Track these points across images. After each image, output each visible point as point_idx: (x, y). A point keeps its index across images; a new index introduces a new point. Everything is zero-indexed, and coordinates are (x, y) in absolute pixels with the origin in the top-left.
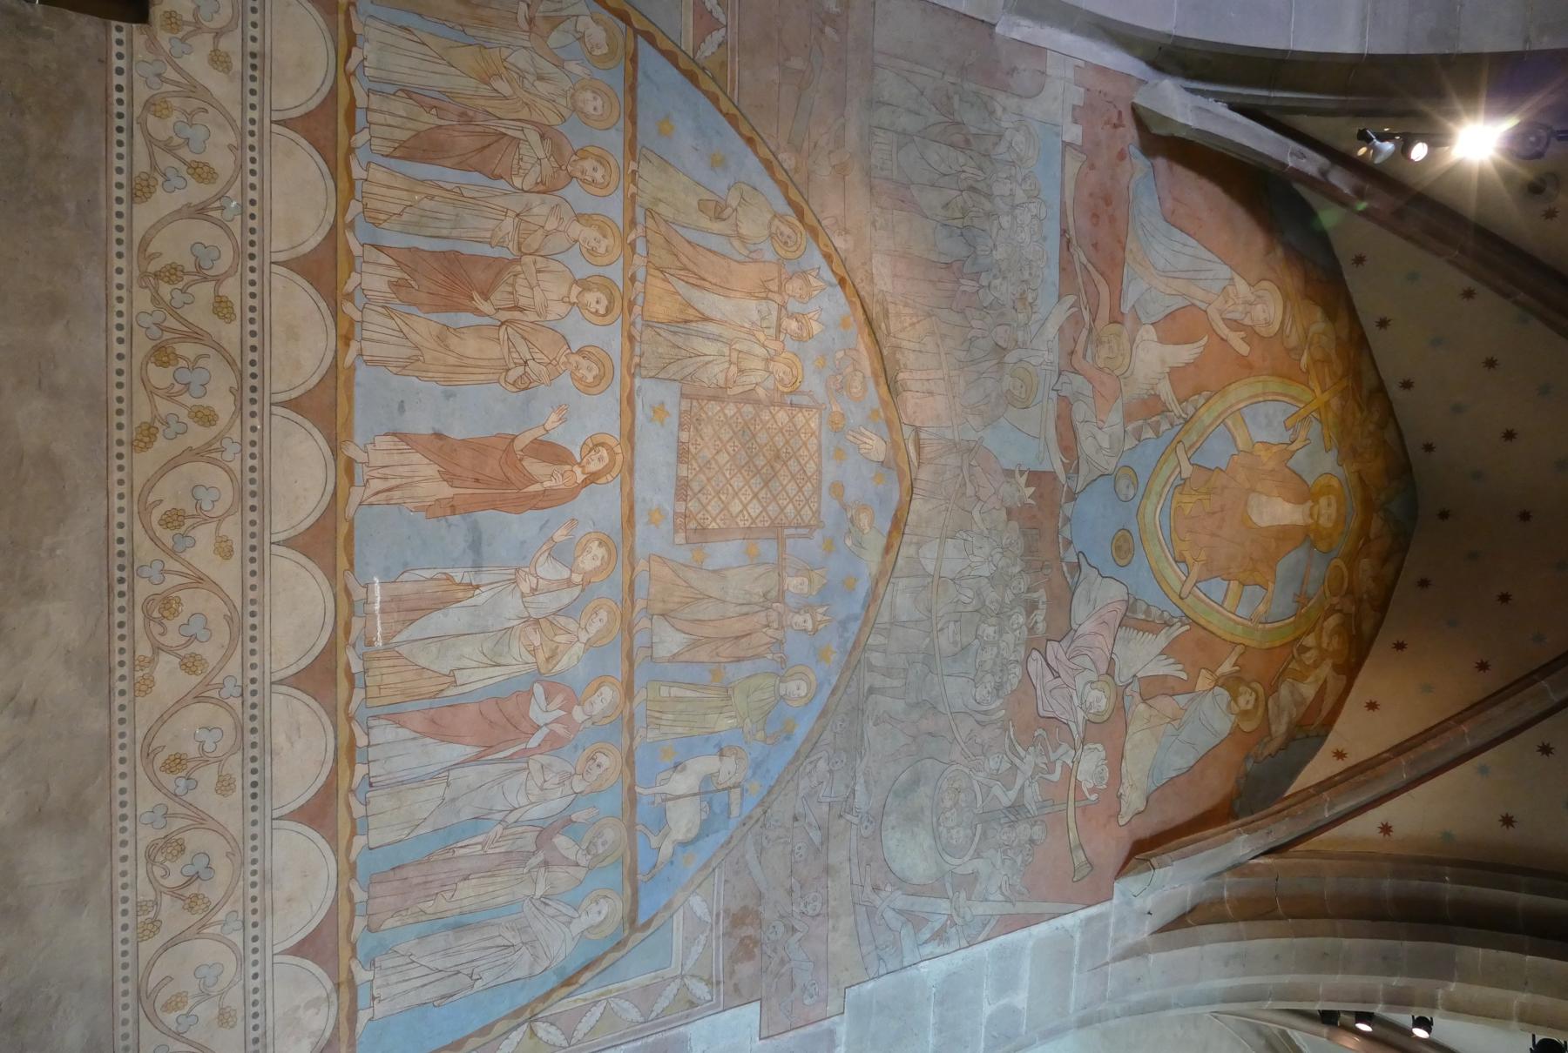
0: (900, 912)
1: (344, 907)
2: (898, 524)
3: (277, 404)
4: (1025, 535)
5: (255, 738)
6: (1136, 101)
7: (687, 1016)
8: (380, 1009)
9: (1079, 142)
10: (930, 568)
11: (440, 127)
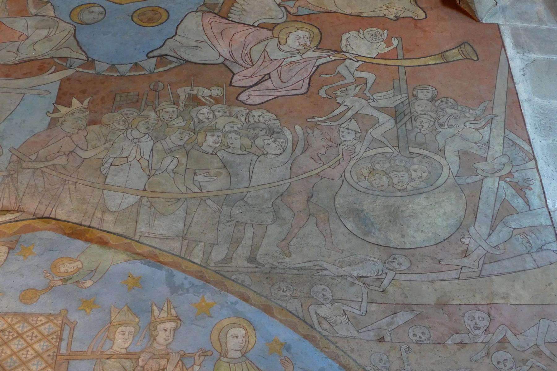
0: (493, 228)
2: (77, 232)
4: (119, 107)
10: (131, 199)
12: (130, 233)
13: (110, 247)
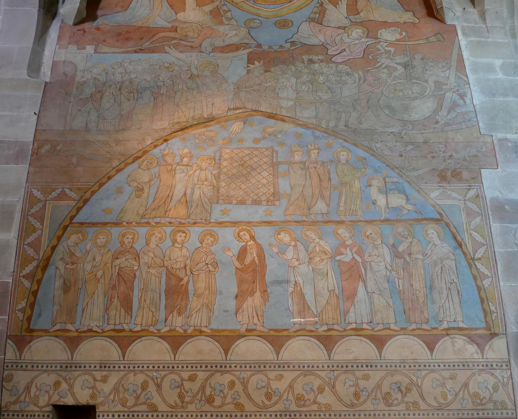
0: (449, 112)
1: (417, 332)
2: (271, 116)
3: (226, 358)
4: (277, 65)
5: (350, 366)
6: (72, 24)
7: (482, 198)
8: (459, 318)
9: (94, 47)
10: (291, 103)
11: (118, 297)
12: (294, 117)
13: (286, 122)
